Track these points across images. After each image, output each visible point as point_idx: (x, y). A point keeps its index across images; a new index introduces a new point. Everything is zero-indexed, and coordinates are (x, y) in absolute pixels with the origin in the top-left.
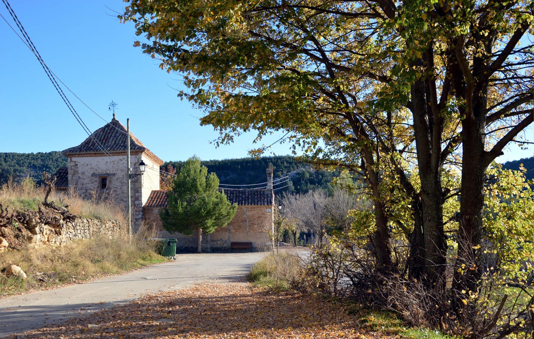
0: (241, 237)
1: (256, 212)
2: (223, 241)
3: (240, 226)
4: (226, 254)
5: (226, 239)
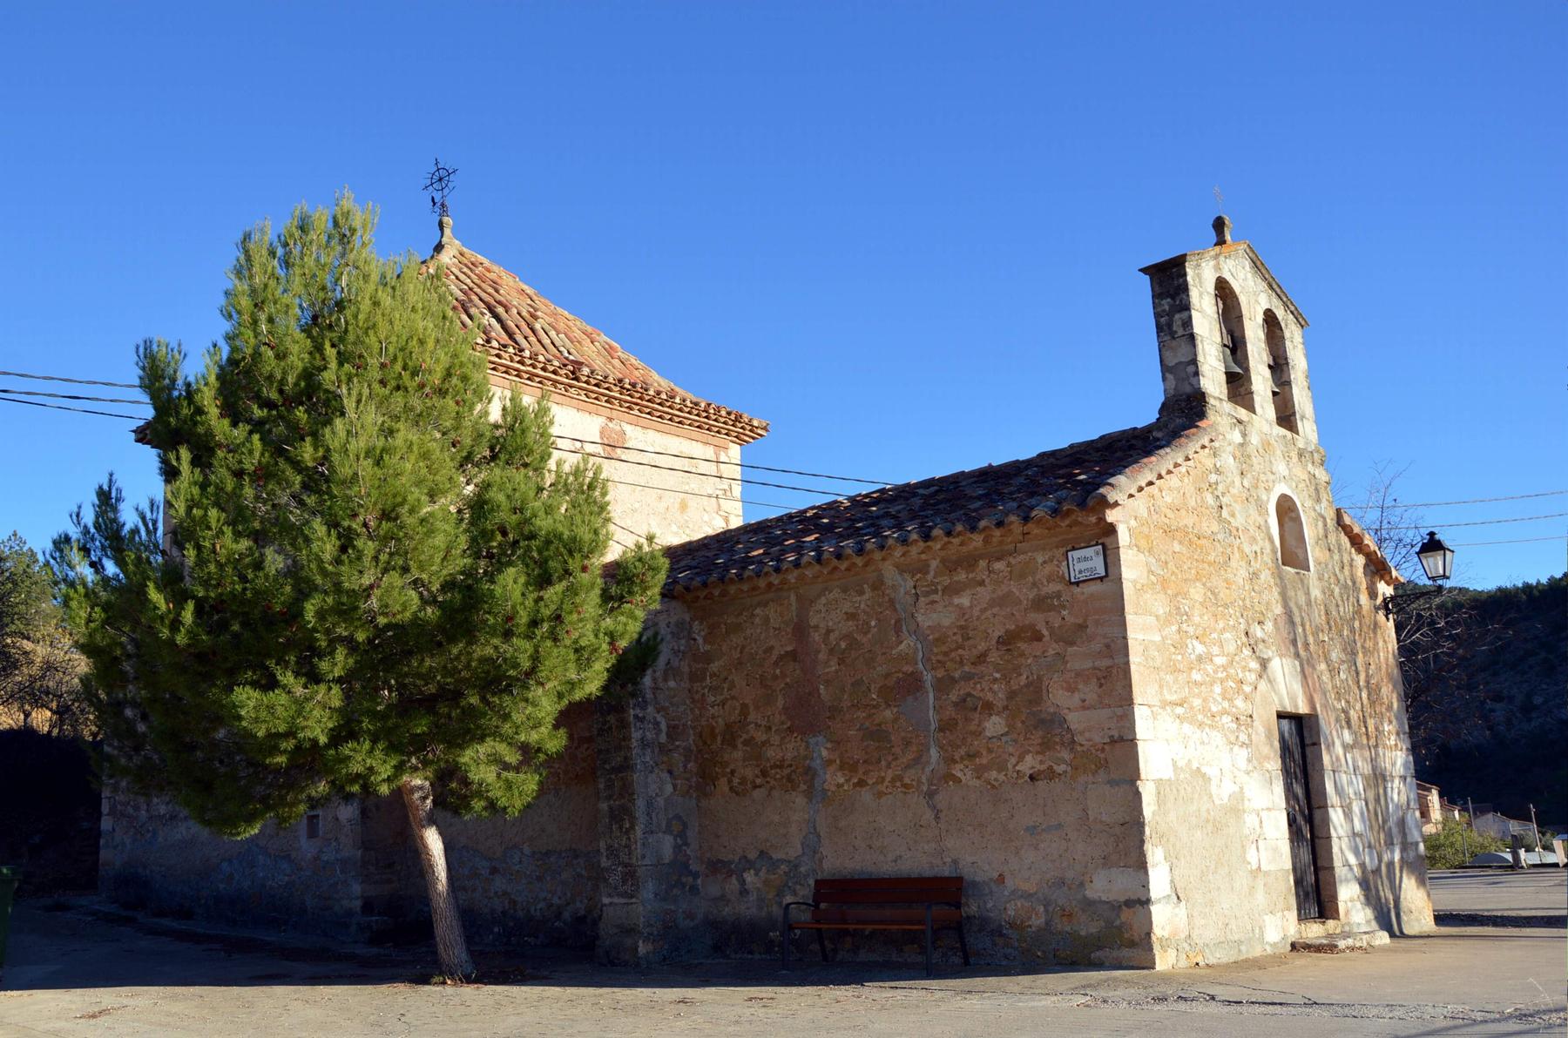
0: (888, 835)
1: (984, 593)
2: (774, 865)
3: (877, 735)
4: (934, 984)
5: (794, 850)
